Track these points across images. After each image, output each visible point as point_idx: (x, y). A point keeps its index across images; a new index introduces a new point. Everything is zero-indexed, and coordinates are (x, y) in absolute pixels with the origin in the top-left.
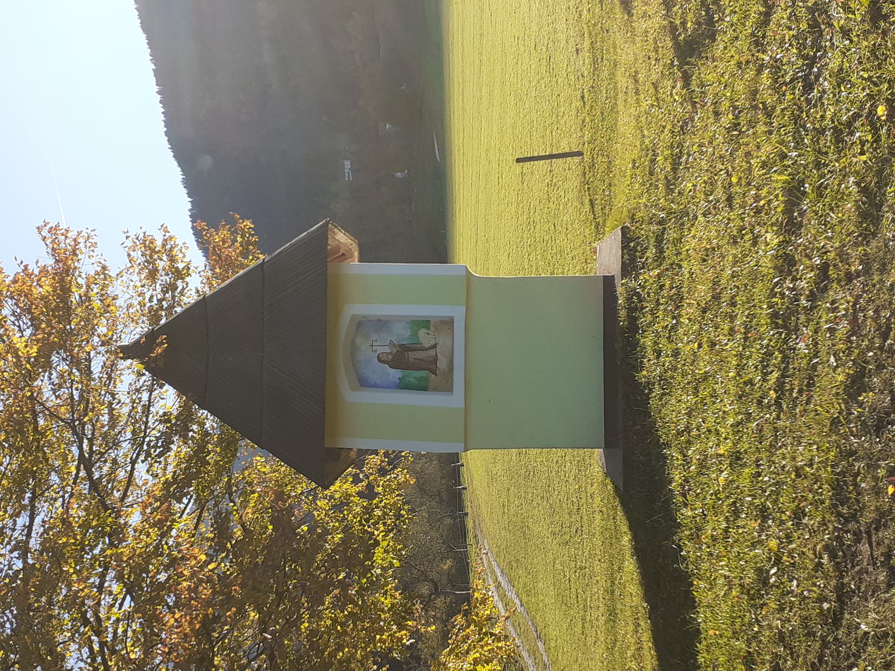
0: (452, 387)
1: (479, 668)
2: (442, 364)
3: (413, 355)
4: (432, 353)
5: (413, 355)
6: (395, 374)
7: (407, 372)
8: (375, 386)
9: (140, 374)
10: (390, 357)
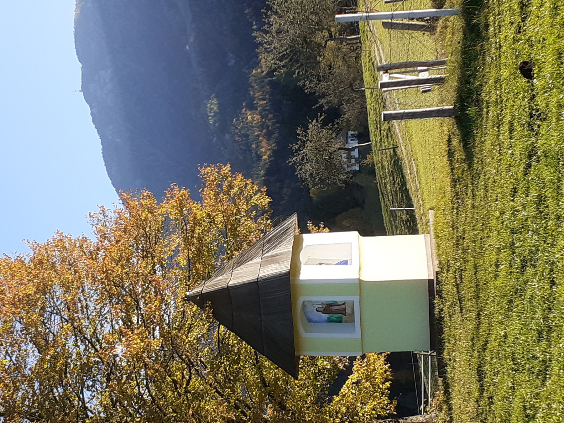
0: (354, 320)
1: (428, 9)
2: (348, 311)
3: (334, 308)
4: (343, 306)
5: (334, 308)
6: (325, 316)
7: (331, 315)
8: (316, 322)
9: (465, 305)
10: (322, 309)
